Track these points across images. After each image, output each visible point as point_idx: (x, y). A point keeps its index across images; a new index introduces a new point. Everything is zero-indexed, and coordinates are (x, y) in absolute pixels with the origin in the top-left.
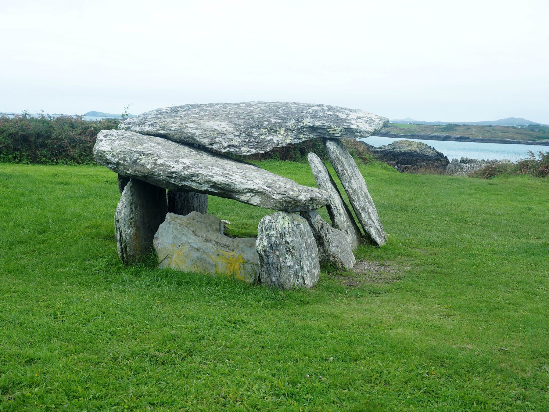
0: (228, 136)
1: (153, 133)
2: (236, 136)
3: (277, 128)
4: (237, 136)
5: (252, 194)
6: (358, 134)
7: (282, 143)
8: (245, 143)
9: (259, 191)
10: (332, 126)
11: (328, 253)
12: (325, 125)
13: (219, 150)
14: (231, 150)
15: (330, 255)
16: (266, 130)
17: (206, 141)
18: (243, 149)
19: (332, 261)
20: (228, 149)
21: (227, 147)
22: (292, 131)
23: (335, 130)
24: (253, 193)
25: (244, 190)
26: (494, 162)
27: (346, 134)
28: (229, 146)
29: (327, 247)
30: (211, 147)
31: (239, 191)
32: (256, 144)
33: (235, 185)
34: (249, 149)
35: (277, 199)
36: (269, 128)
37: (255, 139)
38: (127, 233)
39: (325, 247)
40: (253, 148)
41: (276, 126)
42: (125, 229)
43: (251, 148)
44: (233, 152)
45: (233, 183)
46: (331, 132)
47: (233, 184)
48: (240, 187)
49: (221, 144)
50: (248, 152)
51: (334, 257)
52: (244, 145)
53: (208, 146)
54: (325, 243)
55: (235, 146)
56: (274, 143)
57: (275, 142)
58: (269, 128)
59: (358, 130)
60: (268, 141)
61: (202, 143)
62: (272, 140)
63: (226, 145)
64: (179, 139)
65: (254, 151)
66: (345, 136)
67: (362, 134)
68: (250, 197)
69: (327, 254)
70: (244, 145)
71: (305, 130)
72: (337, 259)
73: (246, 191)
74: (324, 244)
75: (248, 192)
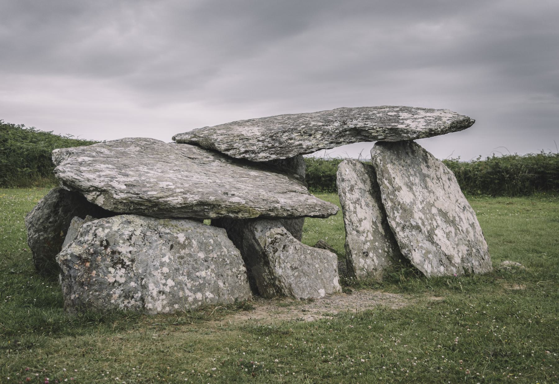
0: (251, 141)
1: (187, 142)
2: (259, 141)
3: (313, 132)
4: (261, 141)
5: (98, 193)
6: (405, 135)
7: (312, 148)
8: (266, 149)
9: (103, 189)
10: (375, 127)
11: (273, 276)
12: (368, 126)
13: (233, 156)
14: (247, 156)
15: (275, 278)
16: (299, 134)
17: (223, 147)
18: (262, 155)
19: (277, 286)
20: (244, 155)
21: (243, 153)
22: (331, 135)
23: (377, 131)
24: (99, 191)
25: (89, 188)
26: (540, 158)
27: (391, 136)
28: (246, 152)
29: (273, 267)
30: (226, 153)
31: (85, 189)
32: (279, 149)
33: (80, 181)
34: (269, 155)
35: (118, 199)
36: (302, 132)
37: (281, 143)
38: (32, 237)
39: (271, 268)
40: (274, 154)
41: (312, 130)
42: (30, 232)
43: (272, 154)
44: (248, 158)
45: (76, 179)
46: (373, 134)
47: (77, 181)
48: (86, 184)
49: (239, 149)
50: (266, 158)
51: (280, 281)
52: (265, 150)
53: (224, 153)
54: (271, 263)
55: (253, 152)
56: (303, 148)
57: (304, 147)
58: (302, 132)
59: (405, 131)
60: (296, 146)
61: (218, 148)
62: (301, 145)
63: (243, 150)
64: (207, 146)
65: (274, 157)
66: (390, 138)
67: (409, 135)
68: (95, 196)
69: (273, 277)
70: (265, 150)
71: (348, 133)
72: (283, 284)
73: (91, 189)
74: (269, 264)
75: (93, 191)
